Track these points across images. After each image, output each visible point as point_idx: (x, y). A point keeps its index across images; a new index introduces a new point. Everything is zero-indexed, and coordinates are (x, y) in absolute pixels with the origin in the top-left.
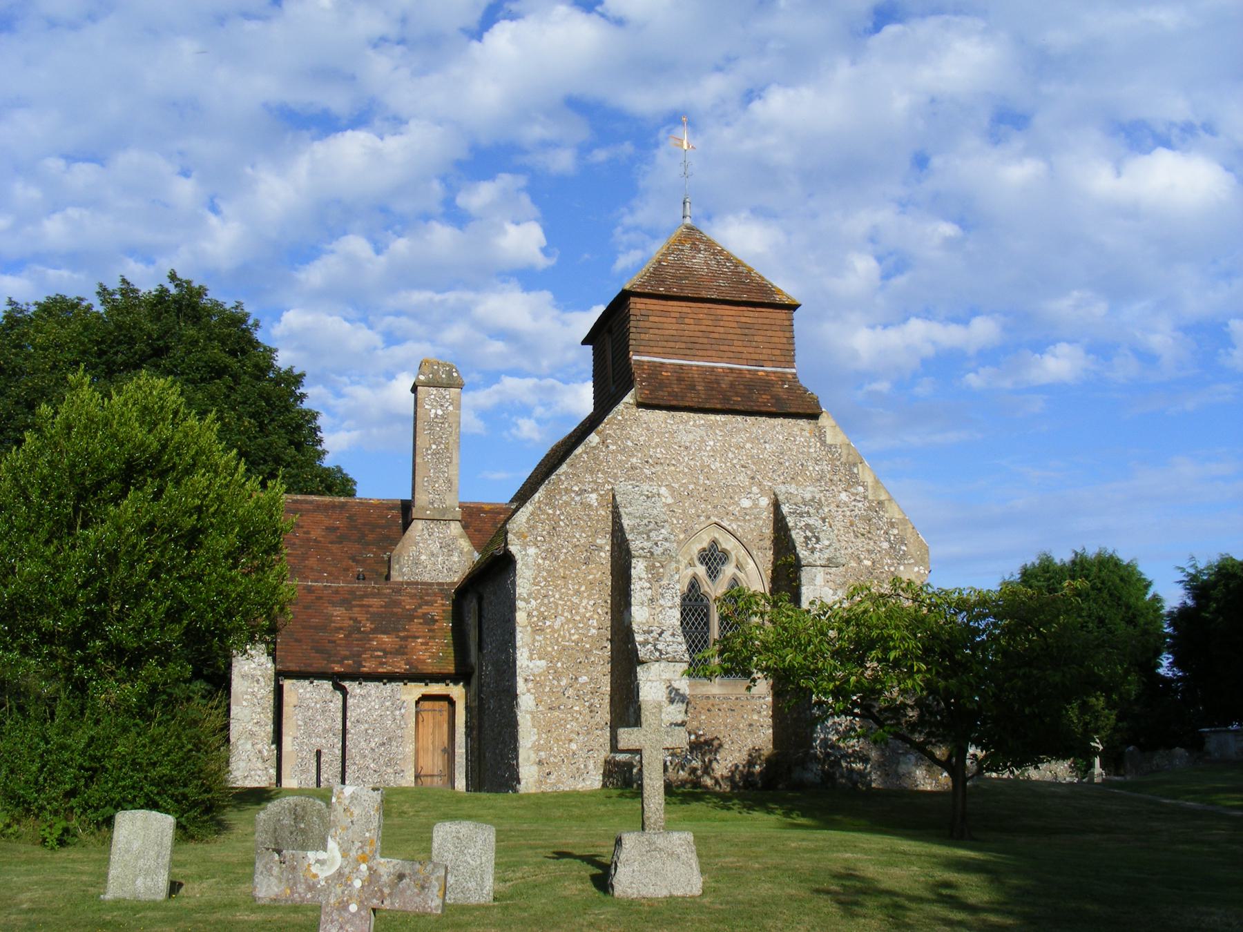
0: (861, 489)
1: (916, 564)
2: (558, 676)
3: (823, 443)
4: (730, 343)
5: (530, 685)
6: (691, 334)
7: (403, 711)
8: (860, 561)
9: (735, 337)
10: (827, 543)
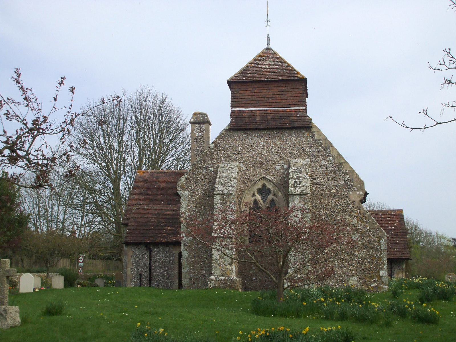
0: (331, 158)
1: (358, 191)
2: (198, 243)
3: (314, 139)
4: (275, 99)
5: (186, 247)
6: (257, 97)
7: (173, 257)
8: (330, 190)
9: (277, 96)
10: (304, 184)
